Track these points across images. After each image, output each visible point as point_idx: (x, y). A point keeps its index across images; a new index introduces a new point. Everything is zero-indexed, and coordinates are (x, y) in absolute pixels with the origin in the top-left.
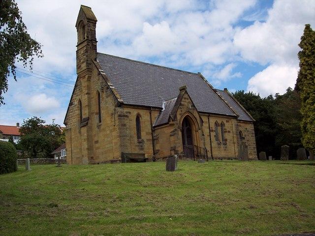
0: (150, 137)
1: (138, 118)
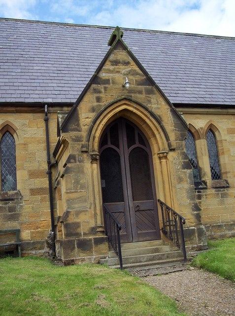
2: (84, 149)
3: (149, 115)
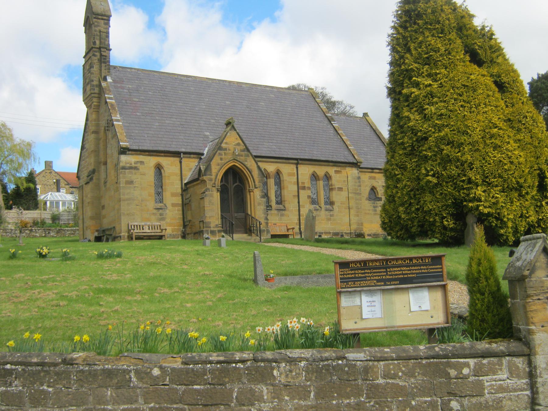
0: (179, 200)
1: (159, 168)
2: (214, 185)
3: (246, 169)
